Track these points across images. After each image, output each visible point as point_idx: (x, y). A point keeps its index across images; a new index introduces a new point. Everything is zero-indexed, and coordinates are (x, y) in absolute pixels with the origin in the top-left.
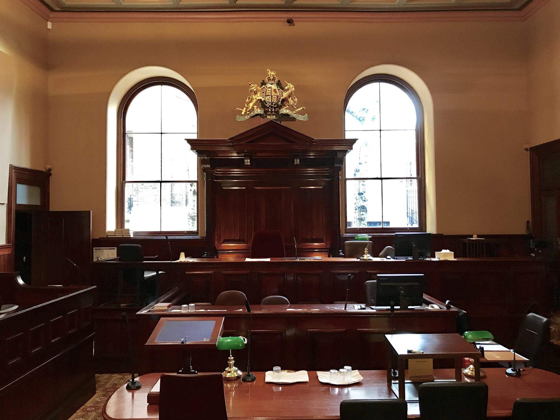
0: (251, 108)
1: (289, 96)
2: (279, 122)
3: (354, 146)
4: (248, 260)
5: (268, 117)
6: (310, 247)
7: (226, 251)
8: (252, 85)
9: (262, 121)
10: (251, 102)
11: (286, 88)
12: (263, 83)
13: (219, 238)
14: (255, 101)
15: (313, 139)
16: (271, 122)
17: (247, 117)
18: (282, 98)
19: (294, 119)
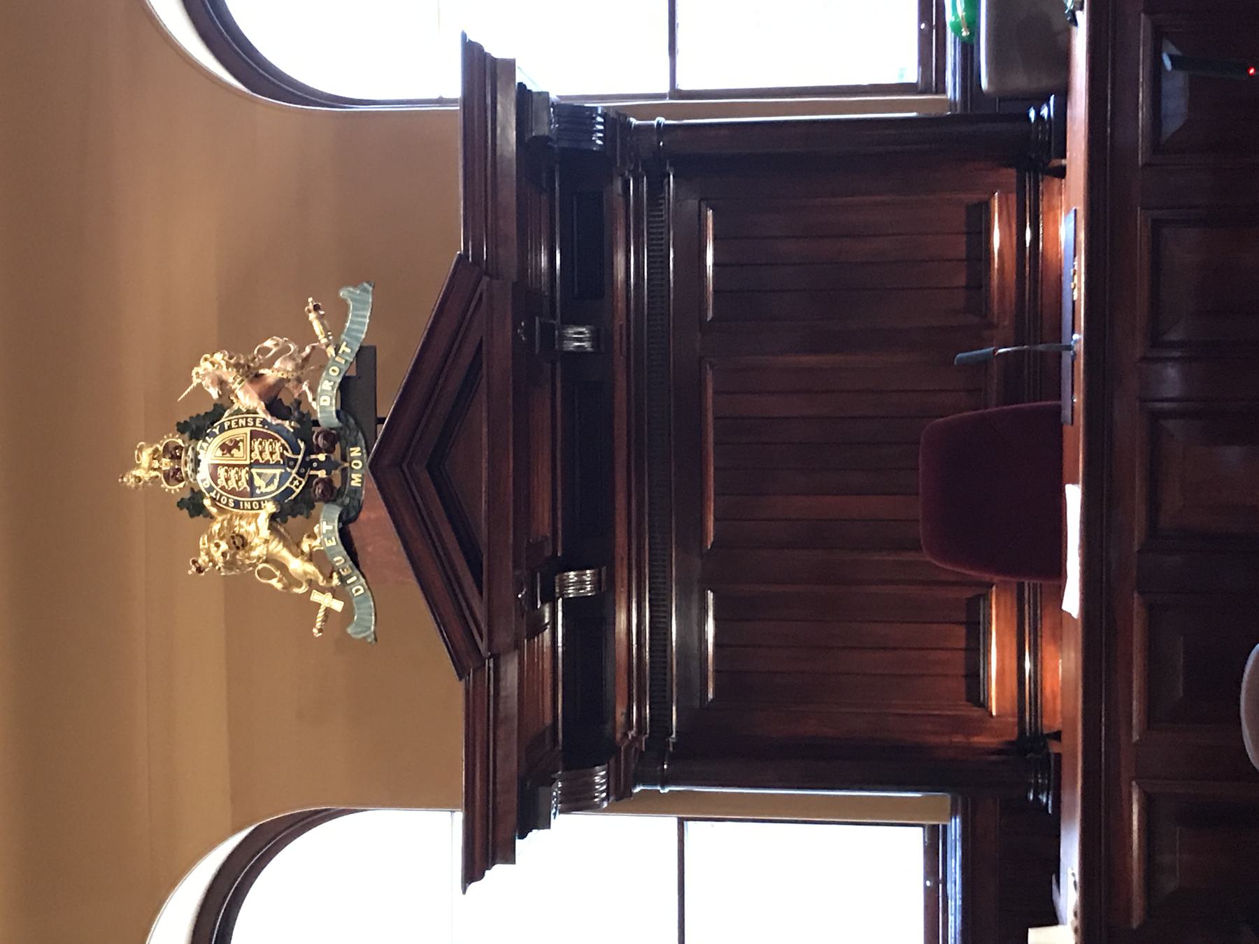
0: (310, 568)
1: (255, 377)
2: (382, 428)
3: (496, 50)
4: (1072, 602)
5: (356, 480)
6: (1011, 265)
7: (1028, 696)
8: (203, 559)
9: (375, 514)
10: (283, 567)
11: (214, 392)
12: (194, 504)
13: (961, 725)
14: (278, 548)
15: (462, 259)
16: (375, 467)
17: (358, 588)
18: (262, 414)
19: (365, 355)
